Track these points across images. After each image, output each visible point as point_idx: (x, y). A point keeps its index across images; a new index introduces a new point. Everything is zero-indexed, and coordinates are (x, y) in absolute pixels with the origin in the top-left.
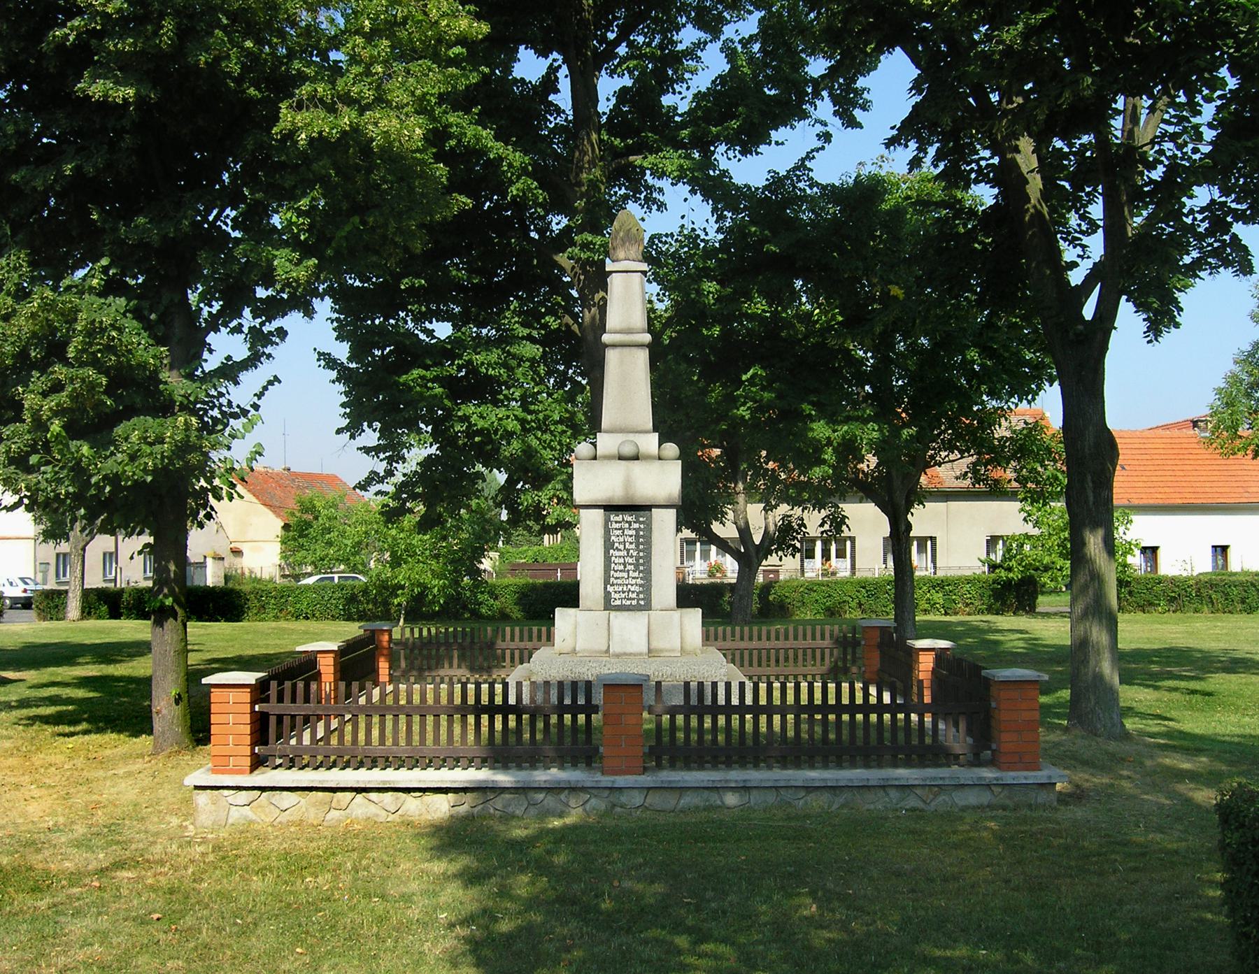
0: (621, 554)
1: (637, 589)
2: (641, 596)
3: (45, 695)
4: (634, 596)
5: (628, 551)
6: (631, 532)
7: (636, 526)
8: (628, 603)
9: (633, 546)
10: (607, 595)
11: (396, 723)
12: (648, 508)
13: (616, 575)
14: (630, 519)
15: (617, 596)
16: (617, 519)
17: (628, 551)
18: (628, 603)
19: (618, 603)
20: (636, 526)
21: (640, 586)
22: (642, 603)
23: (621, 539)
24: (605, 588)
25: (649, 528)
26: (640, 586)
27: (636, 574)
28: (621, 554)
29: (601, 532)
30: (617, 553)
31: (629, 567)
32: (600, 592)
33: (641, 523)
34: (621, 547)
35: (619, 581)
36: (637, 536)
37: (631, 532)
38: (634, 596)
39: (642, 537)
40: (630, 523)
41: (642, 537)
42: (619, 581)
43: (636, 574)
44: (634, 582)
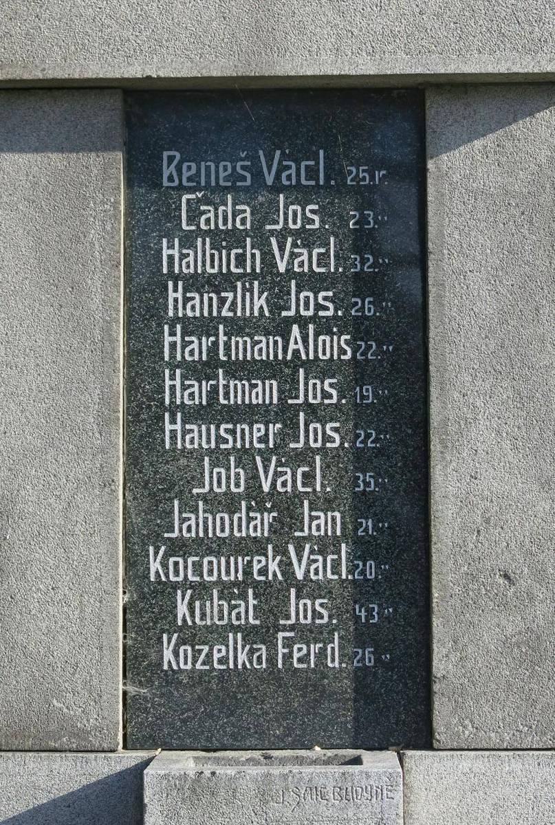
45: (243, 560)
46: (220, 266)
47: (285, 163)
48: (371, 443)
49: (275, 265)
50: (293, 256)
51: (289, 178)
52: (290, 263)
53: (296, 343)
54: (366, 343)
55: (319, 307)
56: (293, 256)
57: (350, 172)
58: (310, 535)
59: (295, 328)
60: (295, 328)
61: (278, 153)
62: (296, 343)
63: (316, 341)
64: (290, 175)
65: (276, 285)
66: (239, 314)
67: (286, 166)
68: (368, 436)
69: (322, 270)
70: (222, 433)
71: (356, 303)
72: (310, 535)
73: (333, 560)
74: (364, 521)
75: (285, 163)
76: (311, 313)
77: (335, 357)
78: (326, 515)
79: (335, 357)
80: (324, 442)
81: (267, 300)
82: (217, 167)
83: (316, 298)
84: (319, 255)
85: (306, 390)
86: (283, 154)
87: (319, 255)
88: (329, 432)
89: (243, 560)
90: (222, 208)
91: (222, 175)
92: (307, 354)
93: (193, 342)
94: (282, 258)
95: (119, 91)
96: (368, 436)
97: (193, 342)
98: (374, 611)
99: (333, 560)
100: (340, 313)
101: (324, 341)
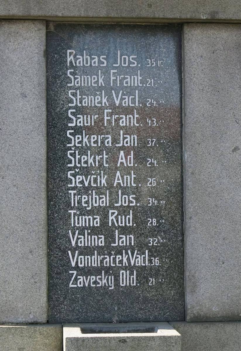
45: (120, 77)
47: (123, 97)
51: (127, 83)
53: (122, 159)
58: (123, 146)
59: (122, 153)
60: (122, 153)
62: (122, 159)
64: (123, 241)
67: (126, 78)
71: (149, 101)
72: (123, 146)
74: (151, 220)
75: (123, 97)
78: (126, 116)
80: (129, 64)
82: (91, 78)
85: (122, 201)
86: (123, 93)
88: (131, 60)
89: (120, 77)
90: (93, 257)
91: (93, 81)
92: (124, 184)
93: (103, 198)
95: (44, 22)
97: (103, 198)
100: (139, 65)
101: (123, 273)
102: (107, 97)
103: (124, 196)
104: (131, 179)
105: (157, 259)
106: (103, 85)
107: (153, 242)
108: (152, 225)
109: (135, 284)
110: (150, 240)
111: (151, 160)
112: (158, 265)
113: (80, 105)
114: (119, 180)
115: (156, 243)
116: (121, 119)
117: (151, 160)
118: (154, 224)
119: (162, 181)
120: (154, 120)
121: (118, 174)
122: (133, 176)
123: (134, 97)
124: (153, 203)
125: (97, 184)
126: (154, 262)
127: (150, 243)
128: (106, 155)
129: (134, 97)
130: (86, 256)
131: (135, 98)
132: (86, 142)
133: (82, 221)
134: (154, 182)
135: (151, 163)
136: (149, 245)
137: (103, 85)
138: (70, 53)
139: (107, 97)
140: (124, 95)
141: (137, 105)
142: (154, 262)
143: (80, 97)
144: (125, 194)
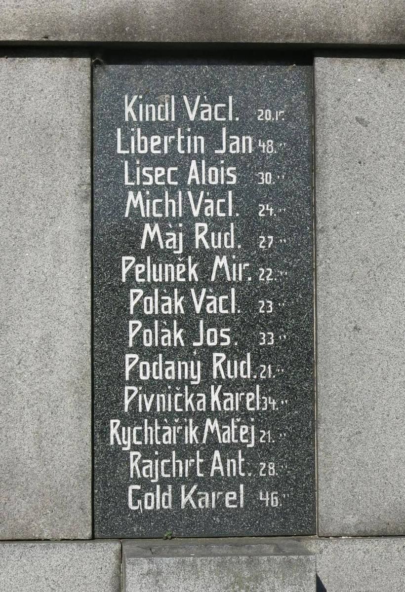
0: (174, 273)
1: (246, 434)
2: (271, 468)
3: (194, 205)
4: (236, 466)
5: (205, 258)
6: (215, 176)
7: (242, 144)
8: (209, 500)
9: (228, 239)
10: (106, 464)
11: (158, 268)
12: (301, 54)
13: (151, 371)
14: (210, 113)
15: (154, 469)
16: (155, 113)
17: (205, 258)
18: (209, 500)
19: (157, 500)
20: (242, 144)
21: (261, 420)
22: (272, 500)
23: (174, 207)
24: (99, 432)
25: (301, 157)
26: (261, 420)
27: (243, 368)
28: (174, 273)
29: (72, 172)
30: (155, 273)
31: (209, 336)
32: (72, 452)
33: (261, 131)
34: (175, 241)
35: (164, 402)
36: (248, 194)
37: (215, 176)
38: (236, 466)
39: (274, 323)
40: (211, 131)
41: (272, 194)
42: (164, 402)
43: (243, 368)
44: (229, 410)
46: (163, 276)
48: (262, 213)
49: (191, 213)
50: (204, 205)
52: (198, 114)
53: (193, 174)
54: (265, 270)
55: (221, 340)
56: (204, 205)
57: (261, 304)
61: (198, 97)
63: (207, 171)
65: (188, 322)
66: (167, 215)
68: (267, 273)
69: (226, 312)
70: (144, 173)
73: (179, 397)
74: (264, 366)
76: (215, 343)
77: (222, 182)
79: (222, 182)
81: (182, 302)
83: (219, 333)
84: (224, 300)
86: (202, 98)
87: (224, 300)
94: (196, 208)
96: (267, 273)
98: (264, 243)
99: (179, 397)
102: (196, 428)
103: (211, 169)
104: (237, 466)
105: (274, 495)
106: (183, 344)
107: (268, 339)
108: (267, 473)
109: (232, 246)
110: (262, 336)
111: (266, 207)
112: (270, 183)
113: (158, 443)
114: (219, 466)
115: (270, 277)
116: (207, 206)
117: (266, 207)
118: (272, 473)
119: (284, 402)
120: (271, 336)
121: (217, 454)
122: (241, 460)
123: (224, 105)
124: (269, 406)
125: (164, 213)
126: (263, 180)
127: (262, 341)
128: (200, 458)
129: (224, 105)
130: (161, 280)
131: (227, 108)
132: (129, 113)
133: (154, 305)
134: (274, 500)
135: (265, 212)
136: (261, 344)
137: (183, 344)
138: (130, 359)
139: (196, 428)
140: (209, 198)
141: (231, 118)
142: (263, 180)
143: (159, 428)
144: (212, 165)
